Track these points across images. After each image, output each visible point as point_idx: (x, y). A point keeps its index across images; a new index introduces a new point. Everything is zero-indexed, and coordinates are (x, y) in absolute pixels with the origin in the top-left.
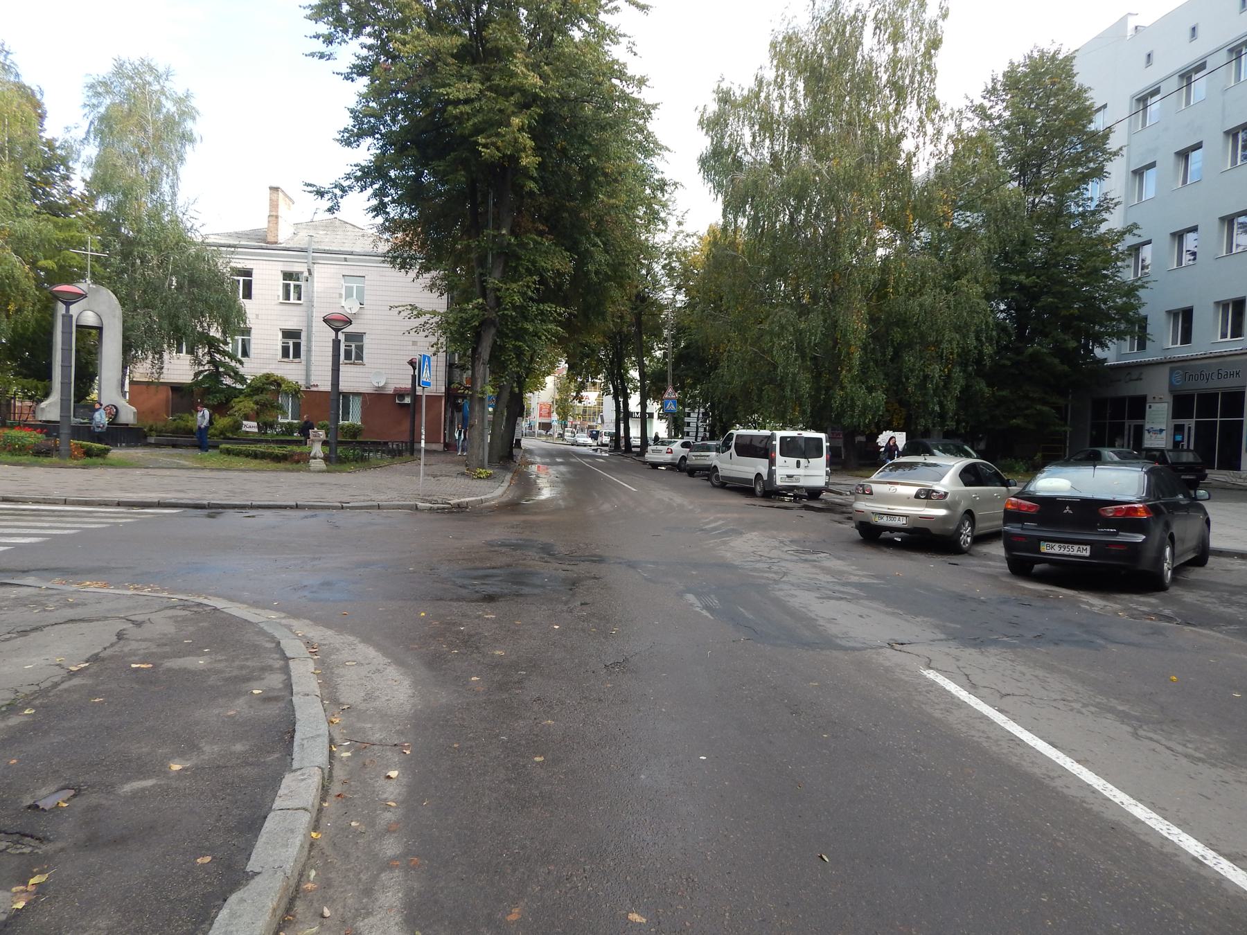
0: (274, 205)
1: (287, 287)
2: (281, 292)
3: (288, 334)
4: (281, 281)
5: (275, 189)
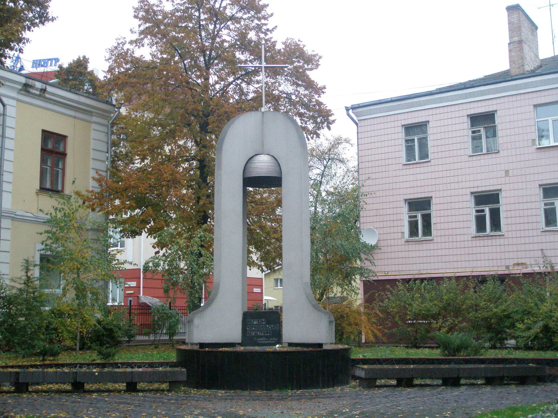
0: (514, 29)
4: (401, 135)
5: (514, 9)
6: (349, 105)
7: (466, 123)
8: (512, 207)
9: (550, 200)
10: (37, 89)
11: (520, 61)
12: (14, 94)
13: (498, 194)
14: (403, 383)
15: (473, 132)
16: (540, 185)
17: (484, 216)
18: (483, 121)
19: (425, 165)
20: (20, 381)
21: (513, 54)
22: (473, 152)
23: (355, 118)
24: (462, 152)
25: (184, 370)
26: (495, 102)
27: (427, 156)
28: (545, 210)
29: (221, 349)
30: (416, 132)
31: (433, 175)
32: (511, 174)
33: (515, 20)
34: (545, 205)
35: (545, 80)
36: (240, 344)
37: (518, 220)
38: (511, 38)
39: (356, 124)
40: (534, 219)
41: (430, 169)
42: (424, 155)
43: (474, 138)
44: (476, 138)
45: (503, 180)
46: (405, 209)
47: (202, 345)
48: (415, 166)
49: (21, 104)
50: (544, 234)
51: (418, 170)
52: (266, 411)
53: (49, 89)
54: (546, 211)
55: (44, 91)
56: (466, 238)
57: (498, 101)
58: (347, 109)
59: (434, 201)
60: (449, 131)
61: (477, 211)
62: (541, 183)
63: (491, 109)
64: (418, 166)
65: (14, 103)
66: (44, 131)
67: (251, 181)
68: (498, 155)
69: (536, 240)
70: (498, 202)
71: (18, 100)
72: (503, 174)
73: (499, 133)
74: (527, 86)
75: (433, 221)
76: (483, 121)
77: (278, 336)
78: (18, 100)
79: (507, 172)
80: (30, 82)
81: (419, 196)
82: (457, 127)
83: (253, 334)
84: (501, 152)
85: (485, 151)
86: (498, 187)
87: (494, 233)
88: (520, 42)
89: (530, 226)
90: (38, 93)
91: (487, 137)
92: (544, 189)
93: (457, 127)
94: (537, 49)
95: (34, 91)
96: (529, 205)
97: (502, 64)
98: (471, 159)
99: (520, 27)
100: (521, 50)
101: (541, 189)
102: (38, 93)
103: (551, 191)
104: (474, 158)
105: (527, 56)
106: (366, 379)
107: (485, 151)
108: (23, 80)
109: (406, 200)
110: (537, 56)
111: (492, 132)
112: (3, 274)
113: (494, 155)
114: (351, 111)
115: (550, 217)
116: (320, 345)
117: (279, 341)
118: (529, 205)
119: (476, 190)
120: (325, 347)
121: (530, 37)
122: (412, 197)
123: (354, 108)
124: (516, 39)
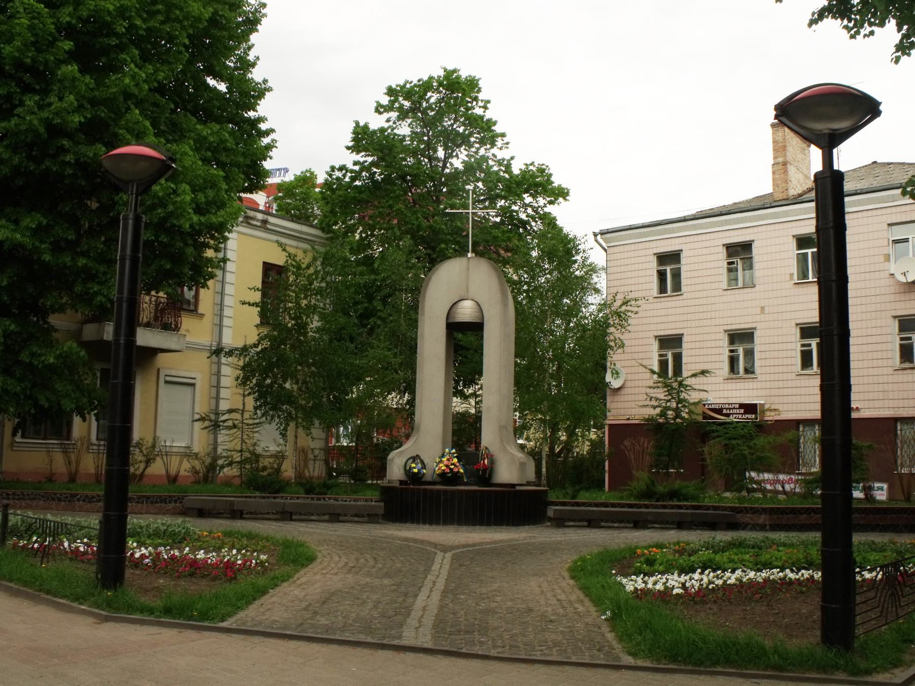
1: (662, 275)
2: (794, 270)
4: (653, 266)
6: (597, 231)
7: (723, 252)
8: (767, 347)
9: (806, 341)
10: (258, 220)
11: (784, 185)
15: (729, 263)
16: (797, 325)
17: (811, 351)
18: (740, 252)
19: (677, 298)
21: (777, 176)
22: (729, 285)
23: (604, 244)
24: (716, 285)
26: (751, 230)
27: (680, 290)
28: (901, 345)
29: (423, 487)
30: (669, 259)
31: (685, 310)
32: (766, 311)
33: (780, 139)
34: (902, 339)
35: (804, 209)
37: (772, 362)
38: (774, 158)
39: (606, 250)
40: (789, 361)
41: (681, 303)
42: (677, 287)
43: (730, 270)
44: (732, 269)
45: (758, 318)
46: (655, 345)
48: (666, 299)
50: (799, 377)
51: (669, 304)
52: (741, 637)
53: (272, 220)
54: (803, 352)
55: (265, 222)
56: (790, 376)
57: (756, 229)
58: (595, 235)
59: (685, 339)
60: (703, 261)
61: (803, 345)
62: (798, 322)
63: (748, 239)
64: (670, 299)
66: (264, 263)
67: (454, 328)
68: (753, 290)
69: (790, 384)
70: (753, 342)
72: (759, 310)
73: (756, 266)
74: (786, 214)
75: (684, 360)
76: (740, 252)
79: (763, 308)
81: (670, 332)
82: (712, 257)
84: (757, 286)
85: (740, 284)
86: (753, 325)
87: (746, 376)
88: (785, 164)
89: (785, 369)
91: (744, 270)
92: (729, 335)
93: (712, 257)
95: (255, 223)
96: (785, 346)
97: (764, 186)
98: (725, 293)
99: (785, 146)
100: (786, 172)
101: (798, 330)
102: (259, 224)
103: (907, 324)
104: (729, 292)
105: (793, 179)
106: (554, 519)
107: (740, 284)
109: (656, 337)
111: (749, 264)
113: (749, 290)
114: (599, 236)
115: (906, 353)
116: (513, 486)
118: (785, 346)
119: (729, 327)
120: (518, 488)
121: (800, 156)
122: (662, 333)
123: (602, 233)
124: (780, 160)
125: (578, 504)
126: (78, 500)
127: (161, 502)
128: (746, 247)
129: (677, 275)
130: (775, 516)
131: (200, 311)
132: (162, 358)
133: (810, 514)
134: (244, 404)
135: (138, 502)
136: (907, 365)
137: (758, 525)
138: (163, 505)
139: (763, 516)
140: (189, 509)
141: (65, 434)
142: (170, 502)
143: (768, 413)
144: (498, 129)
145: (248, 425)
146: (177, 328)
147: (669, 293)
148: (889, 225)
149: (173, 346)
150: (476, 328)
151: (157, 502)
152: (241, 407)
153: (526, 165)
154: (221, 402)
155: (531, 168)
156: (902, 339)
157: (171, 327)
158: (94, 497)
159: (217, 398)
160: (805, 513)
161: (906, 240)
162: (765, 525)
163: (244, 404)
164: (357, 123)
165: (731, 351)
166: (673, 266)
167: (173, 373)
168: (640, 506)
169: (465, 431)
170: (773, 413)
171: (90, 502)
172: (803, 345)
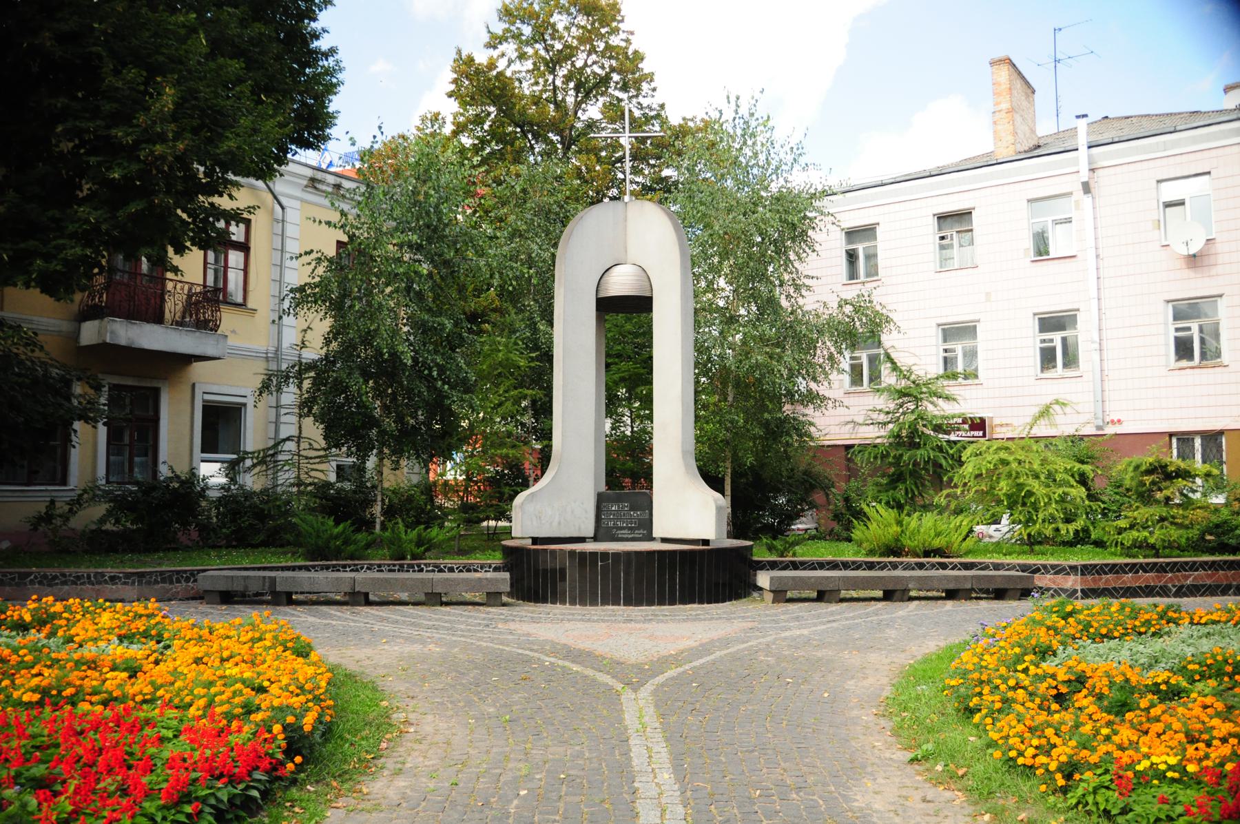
1: (852, 257)
3: (1049, 323)
10: (328, 185)
12: (299, 193)
13: (975, 327)
14: (826, 597)
17: (1054, 349)
20: (278, 589)
25: (507, 575)
34: (1177, 330)
36: (595, 539)
42: (873, 271)
47: (535, 541)
49: (306, 205)
55: (338, 187)
65: (297, 204)
67: (607, 306)
71: (302, 200)
77: (645, 528)
78: (302, 200)
79: (988, 294)
80: (319, 175)
83: (611, 524)
90: (330, 189)
91: (961, 246)
92: (943, 330)
94: (1034, 122)
95: (324, 188)
101: (1037, 322)
102: (330, 189)
108: (309, 173)
110: (1033, 131)
112: (807, 277)
116: (706, 542)
117: (650, 538)
121: (1025, 103)
125: (795, 566)
126: (32, 582)
127: (163, 581)
128: (963, 216)
129: (871, 257)
130: (1089, 578)
131: (250, 305)
132: (198, 370)
133: (1137, 572)
134: (300, 427)
135: (125, 583)
136: (1184, 363)
137: (1064, 591)
138: (167, 586)
139: (1072, 577)
140: (206, 591)
141: (59, 476)
142: (178, 581)
143: (998, 430)
144: (646, 67)
145: (307, 458)
146: (216, 328)
147: (862, 279)
148: (1158, 182)
149: (210, 351)
150: (641, 305)
151: (156, 582)
152: (296, 434)
153: (684, 119)
154: (282, 426)
155: (691, 124)
156: (1177, 330)
157: (207, 326)
158: (55, 577)
159: (277, 423)
160: (1130, 571)
161: (1181, 203)
162: (1075, 591)
163: (300, 427)
164: (459, 52)
165: (946, 351)
166: (867, 244)
167: (215, 389)
168: (883, 567)
169: (628, 470)
170: (1004, 429)
171: (50, 585)
172: (1043, 341)
